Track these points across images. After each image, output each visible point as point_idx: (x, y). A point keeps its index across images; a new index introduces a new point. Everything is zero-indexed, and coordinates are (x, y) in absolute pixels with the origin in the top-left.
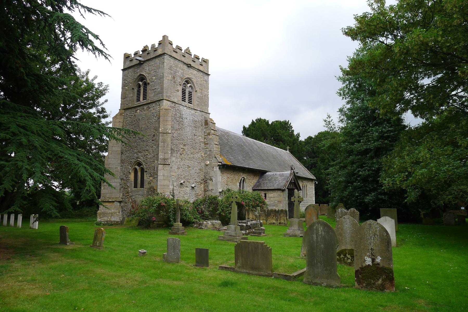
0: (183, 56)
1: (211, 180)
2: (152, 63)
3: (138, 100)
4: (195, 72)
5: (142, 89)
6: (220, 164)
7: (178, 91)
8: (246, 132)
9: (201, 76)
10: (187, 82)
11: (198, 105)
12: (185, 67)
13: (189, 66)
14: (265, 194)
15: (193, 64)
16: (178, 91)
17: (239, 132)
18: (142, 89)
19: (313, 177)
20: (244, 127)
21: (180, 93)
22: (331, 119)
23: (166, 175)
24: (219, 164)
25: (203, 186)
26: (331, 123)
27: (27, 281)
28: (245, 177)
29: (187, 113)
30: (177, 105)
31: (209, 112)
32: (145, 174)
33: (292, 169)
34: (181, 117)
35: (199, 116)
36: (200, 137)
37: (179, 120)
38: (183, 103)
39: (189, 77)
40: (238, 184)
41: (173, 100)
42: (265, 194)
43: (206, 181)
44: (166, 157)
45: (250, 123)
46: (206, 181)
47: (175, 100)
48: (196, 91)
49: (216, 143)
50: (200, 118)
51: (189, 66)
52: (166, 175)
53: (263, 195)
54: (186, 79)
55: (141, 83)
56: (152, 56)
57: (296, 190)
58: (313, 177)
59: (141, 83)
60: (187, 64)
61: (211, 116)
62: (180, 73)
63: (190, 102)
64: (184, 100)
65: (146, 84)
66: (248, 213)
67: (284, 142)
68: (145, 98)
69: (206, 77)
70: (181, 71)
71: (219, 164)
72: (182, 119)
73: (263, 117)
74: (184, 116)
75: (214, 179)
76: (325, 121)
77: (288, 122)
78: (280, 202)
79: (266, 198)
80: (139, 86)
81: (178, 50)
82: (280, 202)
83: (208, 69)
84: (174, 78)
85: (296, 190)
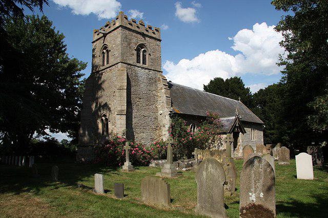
0: (108, 25)
2: (111, 34)
3: (103, 65)
5: (106, 55)
7: (133, 54)
16: (133, 54)
17: (201, 89)
18: (106, 55)
19: (258, 120)
20: (204, 86)
21: (135, 57)
27: (11, 201)
32: (109, 123)
38: (138, 65)
41: (129, 62)
45: (209, 82)
47: (131, 62)
55: (105, 51)
56: (150, 34)
58: (258, 120)
59: (105, 51)
63: (144, 63)
64: (138, 61)
65: (108, 51)
68: (108, 63)
73: (222, 77)
80: (103, 53)
81: (133, 23)
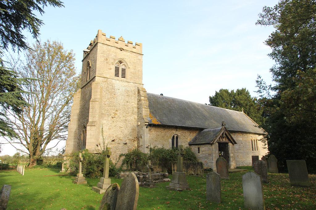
1: (141, 137)
4: (128, 54)
6: (147, 124)
7: (110, 69)
8: (214, 101)
9: (135, 57)
10: (121, 62)
11: (131, 78)
12: (119, 50)
13: (121, 49)
14: (199, 148)
15: (125, 48)
16: (110, 69)
22: (262, 78)
23: (92, 134)
24: (146, 124)
25: (136, 142)
26: (262, 82)
28: (179, 134)
29: (119, 84)
30: (109, 80)
31: (143, 83)
33: (223, 125)
34: (113, 88)
35: (132, 87)
36: (133, 104)
37: (112, 92)
39: (122, 57)
40: (170, 141)
42: (199, 148)
43: (138, 138)
44: (94, 120)
46: (138, 138)
48: (129, 68)
49: (146, 107)
50: (133, 89)
51: (121, 49)
52: (92, 134)
53: (197, 149)
54: (120, 59)
57: (230, 144)
60: (120, 49)
61: (144, 87)
62: (112, 56)
66: (174, 165)
67: (240, 105)
69: (140, 57)
70: (113, 54)
71: (146, 124)
72: (115, 89)
74: (116, 88)
75: (143, 137)
76: (257, 82)
77: (245, 89)
78: (210, 155)
79: (199, 152)
82: (210, 155)
83: (141, 50)
84: (107, 59)
85: (230, 144)
